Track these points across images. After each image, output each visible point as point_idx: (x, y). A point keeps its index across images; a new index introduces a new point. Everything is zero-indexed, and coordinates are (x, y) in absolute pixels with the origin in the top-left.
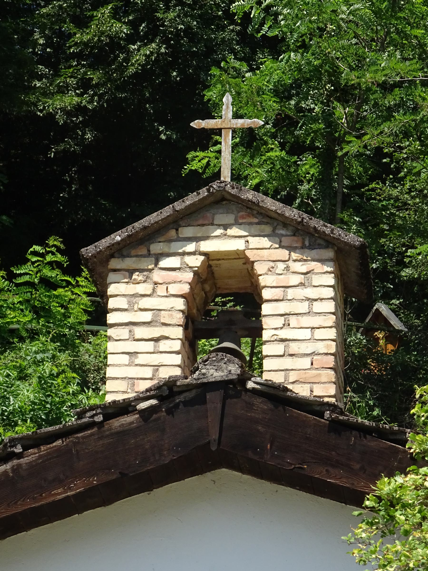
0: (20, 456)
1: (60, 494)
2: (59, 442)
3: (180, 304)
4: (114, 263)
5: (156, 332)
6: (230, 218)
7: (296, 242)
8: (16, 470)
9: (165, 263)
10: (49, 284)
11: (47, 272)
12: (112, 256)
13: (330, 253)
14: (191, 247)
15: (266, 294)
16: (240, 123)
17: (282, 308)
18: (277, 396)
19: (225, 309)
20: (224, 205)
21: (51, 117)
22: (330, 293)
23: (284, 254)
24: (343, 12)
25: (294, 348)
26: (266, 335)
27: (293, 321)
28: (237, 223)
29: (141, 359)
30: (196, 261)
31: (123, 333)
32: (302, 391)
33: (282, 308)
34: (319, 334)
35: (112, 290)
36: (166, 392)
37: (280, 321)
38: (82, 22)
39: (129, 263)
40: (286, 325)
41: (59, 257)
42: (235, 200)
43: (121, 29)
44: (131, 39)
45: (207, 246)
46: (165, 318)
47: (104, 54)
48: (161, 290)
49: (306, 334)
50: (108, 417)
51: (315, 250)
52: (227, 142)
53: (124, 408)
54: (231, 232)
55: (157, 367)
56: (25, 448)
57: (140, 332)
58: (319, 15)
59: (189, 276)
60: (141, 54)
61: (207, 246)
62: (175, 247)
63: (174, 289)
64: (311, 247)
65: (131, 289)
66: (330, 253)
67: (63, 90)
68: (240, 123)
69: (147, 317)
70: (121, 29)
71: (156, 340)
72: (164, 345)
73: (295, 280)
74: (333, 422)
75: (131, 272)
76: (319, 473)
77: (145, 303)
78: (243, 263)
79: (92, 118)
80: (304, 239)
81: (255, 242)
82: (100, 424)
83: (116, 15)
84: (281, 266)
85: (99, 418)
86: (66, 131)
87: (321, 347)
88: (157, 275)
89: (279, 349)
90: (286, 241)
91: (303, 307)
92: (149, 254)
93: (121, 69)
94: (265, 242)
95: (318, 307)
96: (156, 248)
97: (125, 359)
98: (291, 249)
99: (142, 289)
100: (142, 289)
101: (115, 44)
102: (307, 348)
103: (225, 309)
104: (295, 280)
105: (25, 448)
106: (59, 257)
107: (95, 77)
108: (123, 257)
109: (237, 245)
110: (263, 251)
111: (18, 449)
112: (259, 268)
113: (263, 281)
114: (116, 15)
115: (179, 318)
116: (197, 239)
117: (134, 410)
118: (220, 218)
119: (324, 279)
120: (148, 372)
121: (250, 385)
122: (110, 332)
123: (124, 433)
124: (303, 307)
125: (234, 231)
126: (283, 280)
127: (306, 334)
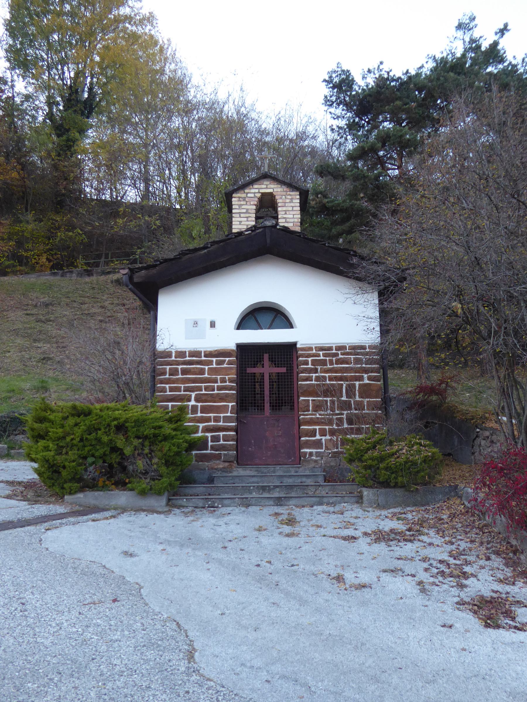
5: (247, 215)
8: (208, 252)
17: (284, 209)
18: (286, 230)
25: (288, 220)
29: (243, 223)
32: (292, 229)
33: (284, 209)
36: (253, 228)
37: (284, 213)
40: (286, 214)
51: (125, 517)
53: (240, 234)
55: (247, 225)
57: (242, 215)
58: (468, 168)
63: (252, 203)
69: (244, 211)
71: (247, 217)
76: (249, 463)
87: (296, 220)
89: (284, 220)
102: (292, 220)
112: (277, 197)
113: (278, 201)
121: (278, 227)
124: (291, 209)
127: (292, 216)
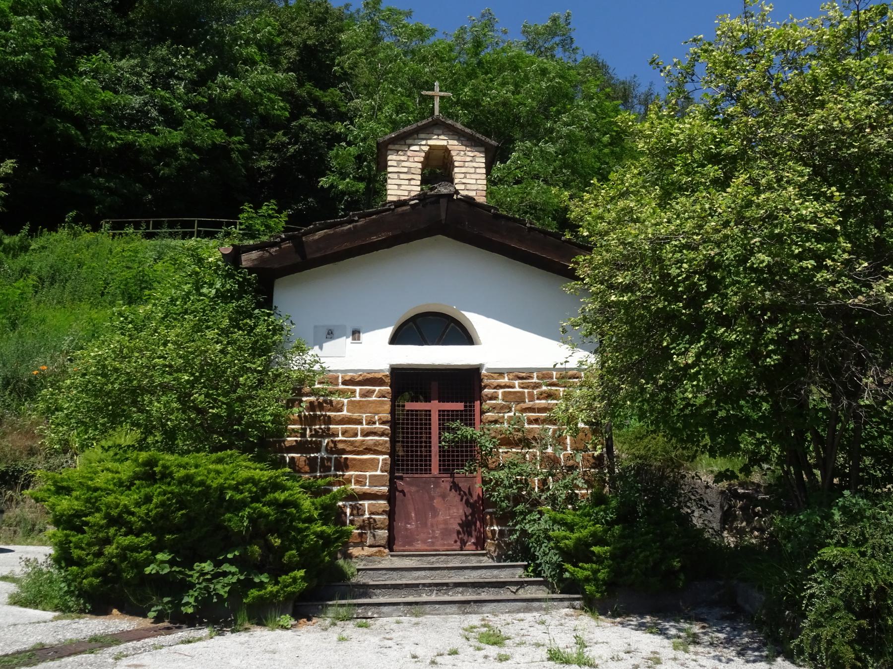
0: (357, 221)
1: (374, 239)
3: (420, 165)
4: (390, 147)
5: (410, 176)
6: (440, 132)
7: (469, 143)
9: (413, 148)
10: (270, 216)
11: (270, 212)
12: (389, 144)
13: (483, 149)
14: (424, 142)
15: (456, 164)
16: (442, 94)
17: (463, 170)
19: (438, 169)
20: (436, 126)
21: (259, 168)
22: (483, 165)
23: (463, 148)
25: (469, 187)
26: (456, 181)
27: (468, 176)
28: (443, 134)
29: (403, 187)
30: (426, 148)
31: (395, 176)
33: (463, 170)
34: (479, 182)
35: (389, 158)
37: (462, 176)
38: (272, 137)
39: (397, 147)
40: (465, 177)
41: (274, 207)
43: (285, 139)
44: (289, 144)
45: (430, 142)
46: (413, 171)
47: (279, 148)
48: (411, 159)
49: (474, 181)
50: (396, 207)
52: (437, 102)
53: (400, 203)
54: (441, 137)
56: (359, 218)
57: (402, 176)
59: (423, 154)
60: (292, 149)
61: (430, 142)
62: (416, 142)
63: (416, 159)
64: (475, 146)
65: (398, 158)
66: (483, 149)
67: (264, 159)
68: (442, 94)
69: (405, 170)
70: (285, 139)
71: (410, 180)
72: (413, 182)
73: (469, 159)
74: (494, 214)
75: (398, 151)
77: (404, 164)
78: (446, 150)
79: (273, 170)
80: (471, 142)
81: (451, 142)
82: (393, 210)
83: (284, 134)
84: (462, 153)
85: (393, 207)
86: (265, 174)
87: (480, 187)
88: (409, 153)
90: (464, 143)
91: (472, 170)
92: (405, 144)
93: (285, 154)
94: (455, 142)
95: (478, 171)
96: (409, 141)
97: (396, 187)
98: (466, 146)
99: (402, 158)
100: (402, 158)
101: (284, 145)
102: (475, 187)
103: (438, 169)
104: (469, 159)
105: (359, 218)
106: (274, 207)
107: (276, 155)
109: (444, 143)
110: (453, 145)
111: (356, 218)
112: (453, 153)
114: (284, 134)
115: (419, 171)
116: (426, 139)
117: (408, 204)
118: (436, 131)
119: (481, 160)
120: (406, 193)
122: (389, 175)
123: (403, 214)
124: (472, 170)
125: (442, 137)
126: (463, 159)
127: (474, 181)
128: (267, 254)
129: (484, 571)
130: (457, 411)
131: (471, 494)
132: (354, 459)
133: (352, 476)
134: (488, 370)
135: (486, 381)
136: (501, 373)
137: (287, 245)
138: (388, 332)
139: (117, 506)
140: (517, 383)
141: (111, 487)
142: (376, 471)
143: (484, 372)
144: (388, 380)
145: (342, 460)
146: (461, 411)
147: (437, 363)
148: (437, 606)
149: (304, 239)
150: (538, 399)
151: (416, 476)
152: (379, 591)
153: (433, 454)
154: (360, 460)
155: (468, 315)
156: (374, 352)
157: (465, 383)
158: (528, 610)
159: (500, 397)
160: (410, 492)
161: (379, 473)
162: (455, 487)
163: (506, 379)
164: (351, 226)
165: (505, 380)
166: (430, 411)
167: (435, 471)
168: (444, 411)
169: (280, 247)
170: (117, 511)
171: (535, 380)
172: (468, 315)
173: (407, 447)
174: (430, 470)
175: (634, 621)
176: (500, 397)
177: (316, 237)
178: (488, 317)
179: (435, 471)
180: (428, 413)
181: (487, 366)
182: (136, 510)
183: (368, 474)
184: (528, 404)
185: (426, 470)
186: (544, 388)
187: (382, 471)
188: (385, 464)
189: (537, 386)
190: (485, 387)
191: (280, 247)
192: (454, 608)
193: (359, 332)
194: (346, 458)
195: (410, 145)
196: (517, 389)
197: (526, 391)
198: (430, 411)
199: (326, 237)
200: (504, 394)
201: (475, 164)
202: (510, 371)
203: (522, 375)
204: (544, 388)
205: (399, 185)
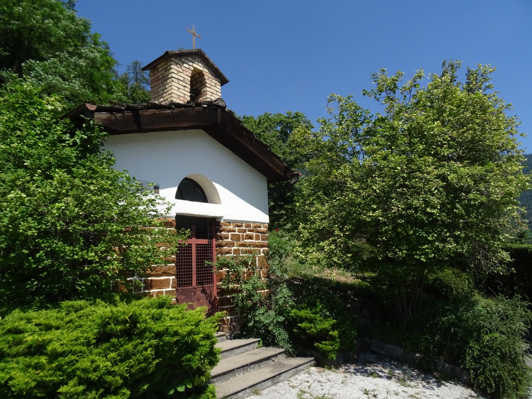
0: (173, 109)
2: (183, 109)
4: (173, 59)
5: (185, 85)
9: (185, 65)
14: (191, 64)
18: (173, 105)
23: (210, 76)
24: (27, 88)
29: (181, 90)
35: (172, 66)
39: (176, 61)
42: (157, 63)
45: (195, 65)
61: (195, 65)
62: (187, 62)
63: (188, 74)
71: (184, 86)
75: (177, 64)
77: (181, 74)
92: (181, 60)
94: (207, 71)
96: (183, 60)
97: (177, 89)
100: (180, 70)
108: (175, 58)
109: (201, 68)
111: (173, 107)
116: (193, 63)
117: (201, 106)
118: (197, 59)
125: (200, 64)
128: (113, 118)
129: (242, 348)
130: (204, 245)
131: (211, 296)
132: (156, 280)
133: (154, 292)
134: (225, 220)
135: (224, 227)
136: (229, 222)
137: (128, 114)
138: (175, 190)
139: (96, 370)
140: (236, 229)
141: (77, 348)
142: (169, 288)
143: (222, 221)
144: (174, 224)
145: (149, 282)
146: (207, 245)
147: (201, 214)
148: (263, 383)
149: (140, 112)
150: (246, 239)
151: (185, 288)
152: (215, 379)
153: (193, 273)
154: (160, 281)
155: (217, 185)
156: (170, 203)
157: (209, 227)
158: (297, 373)
159: (230, 237)
160: (181, 299)
161: (170, 289)
162: (204, 291)
163: (232, 227)
164: (169, 111)
165: (231, 227)
166: (191, 244)
167: (194, 284)
168: (198, 244)
169: (123, 114)
170: (98, 374)
171: (244, 228)
172: (217, 185)
173: (180, 269)
174: (192, 283)
175: (352, 368)
176: (230, 237)
177: (148, 113)
178: (225, 187)
179: (194, 284)
180: (190, 245)
181: (226, 217)
182: (116, 368)
183: (164, 290)
184: (241, 242)
185: (189, 284)
186: (248, 233)
187: (172, 288)
188: (174, 283)
189: (245, 231)
190: (222, 231)
191: (123, 114)
192: (269, 383)
193: (158, 188)
194: (151, 280)
195: (183, 63)
196: (237, 233)
197: (241, 234)
198: (191, 244)
199: (154, 115)
200: (232, 235)
201: (216, 89)
202: (234, 222)
203: (238, 224)
204: (248, 233)
205: (179, 88)
